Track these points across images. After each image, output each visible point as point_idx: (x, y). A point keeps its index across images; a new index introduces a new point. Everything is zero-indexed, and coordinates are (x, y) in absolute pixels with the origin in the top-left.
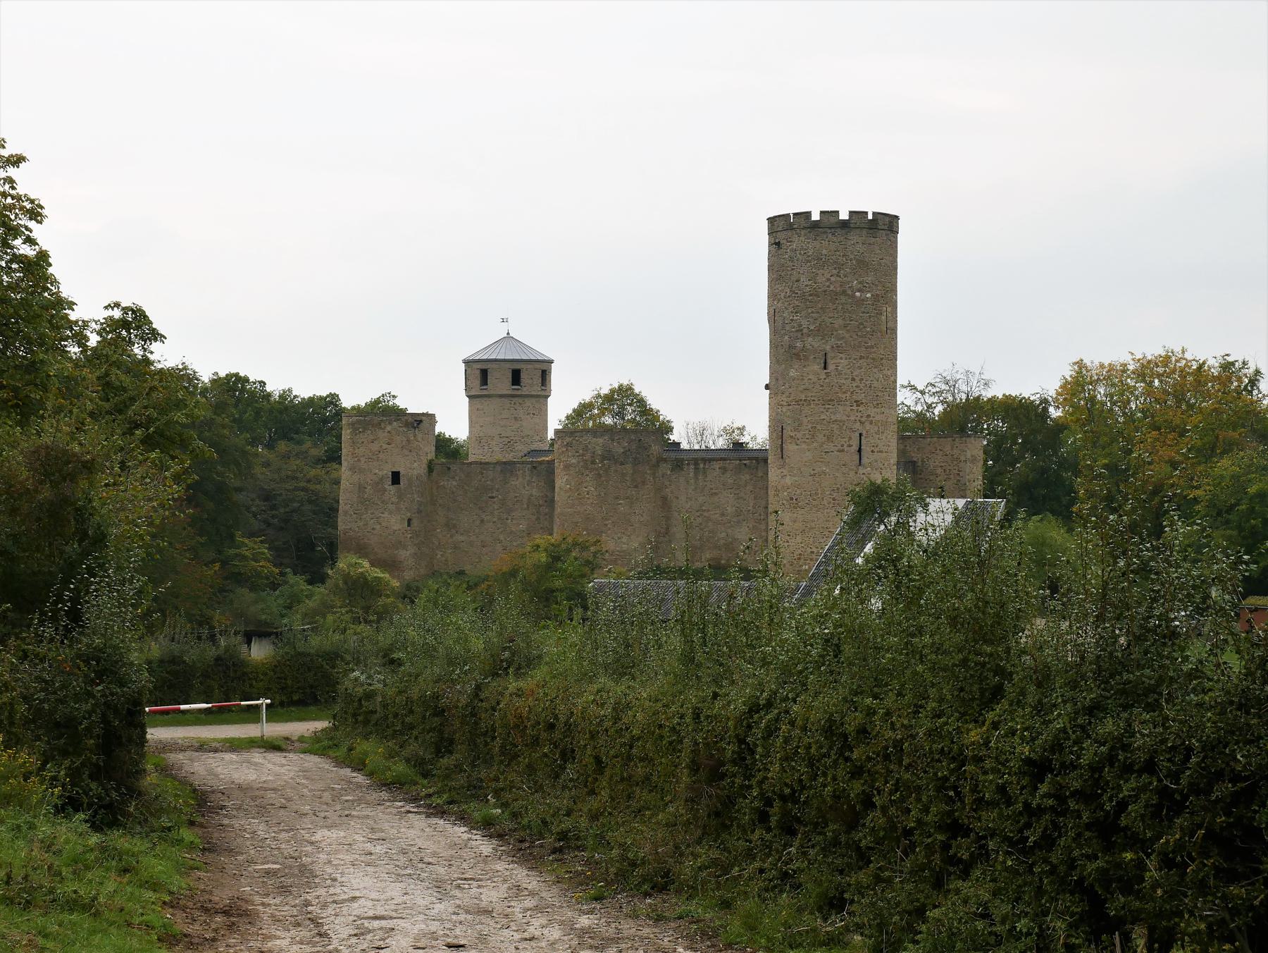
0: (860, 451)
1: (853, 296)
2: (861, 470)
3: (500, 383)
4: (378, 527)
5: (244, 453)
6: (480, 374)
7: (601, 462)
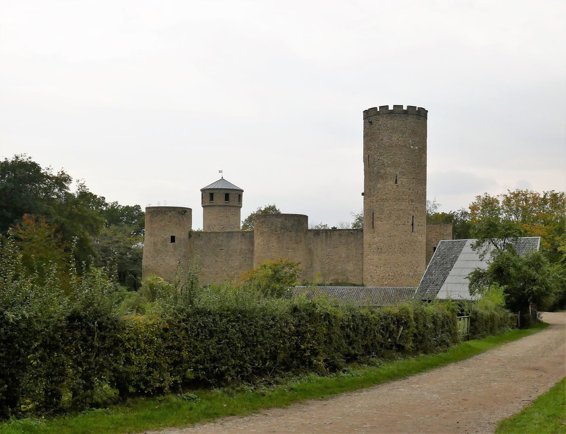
0: (412, 225)
1: (410, 148)
2: (413, 234)
3: (219, 200)
4: (163, 264)
5: (95, 220)
6: (209, 195)
7: (280, 230)
